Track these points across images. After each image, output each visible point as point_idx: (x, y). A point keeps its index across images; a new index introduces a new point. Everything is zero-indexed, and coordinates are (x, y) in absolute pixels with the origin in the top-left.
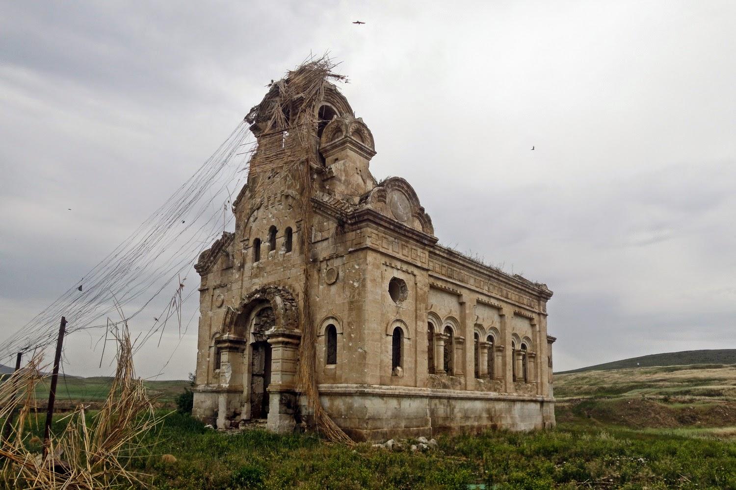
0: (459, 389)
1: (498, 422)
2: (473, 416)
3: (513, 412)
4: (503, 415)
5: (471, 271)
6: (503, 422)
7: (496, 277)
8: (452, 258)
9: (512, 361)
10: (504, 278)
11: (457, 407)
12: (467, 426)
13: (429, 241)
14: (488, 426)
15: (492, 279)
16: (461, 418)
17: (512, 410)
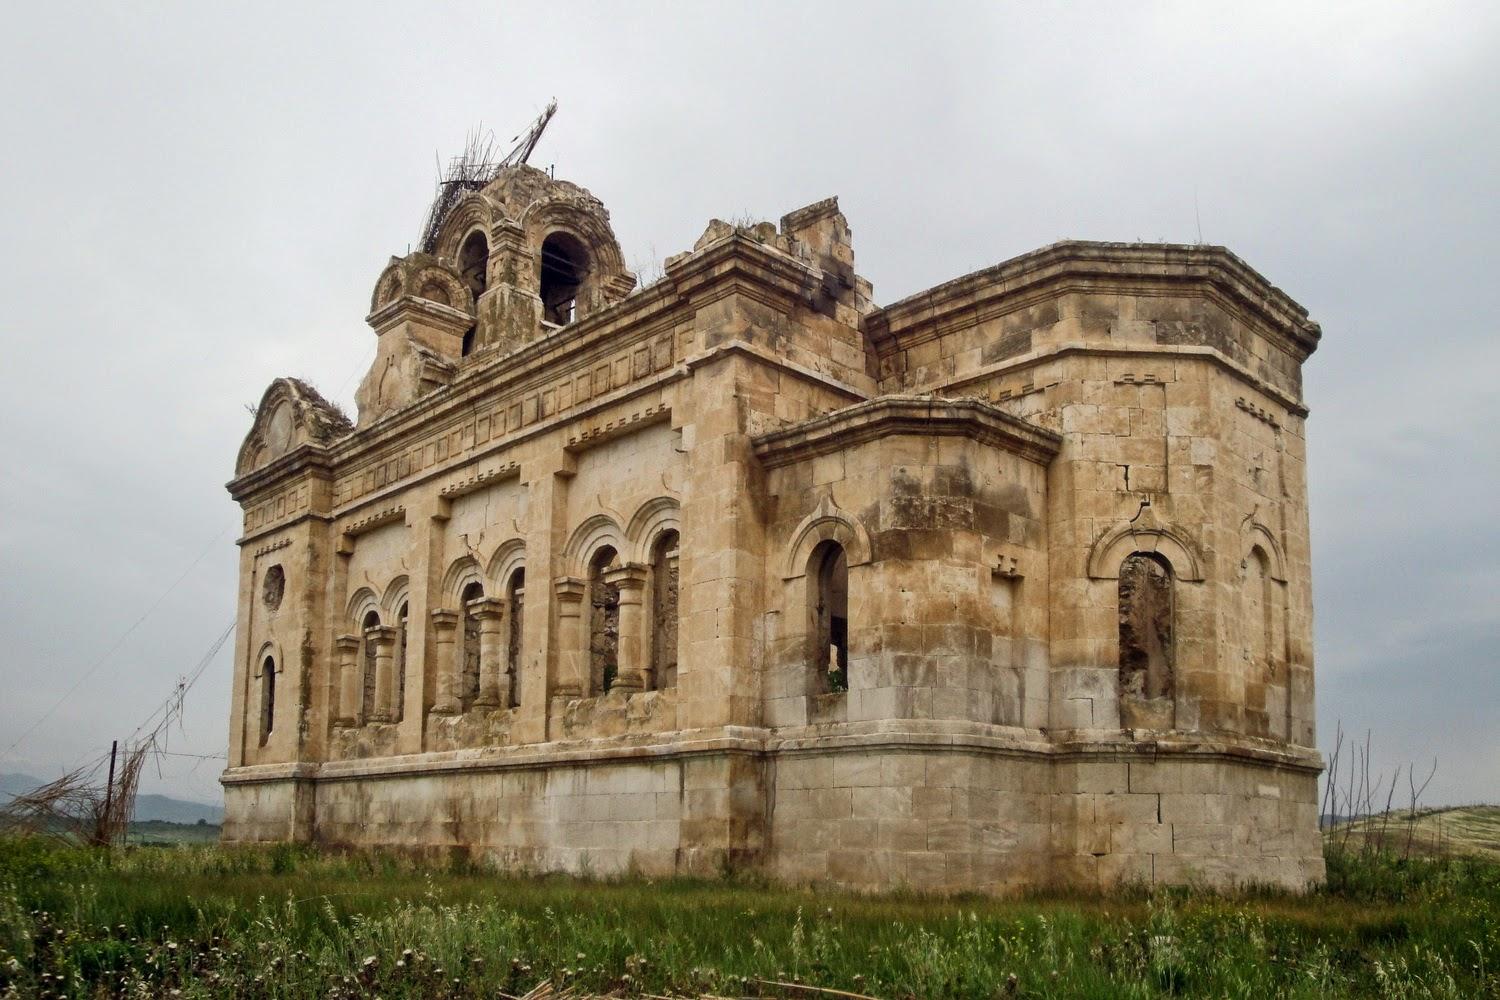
0: (734, 847)
1: (476, 838)
2: (409, 820)
3: (539, 808)
4: (502, 819)
5: (1130, 285)
6: (496, 840)
7: (481, 389)
8: (373, 443)
9: (545, 630)
10: (504, 371)
11: (1254, 872)
12: (389, 845)
13: (300, 458)
14: (442, 849)
15: (482, 403)
16: (380, 825)
17: (537, 799)
